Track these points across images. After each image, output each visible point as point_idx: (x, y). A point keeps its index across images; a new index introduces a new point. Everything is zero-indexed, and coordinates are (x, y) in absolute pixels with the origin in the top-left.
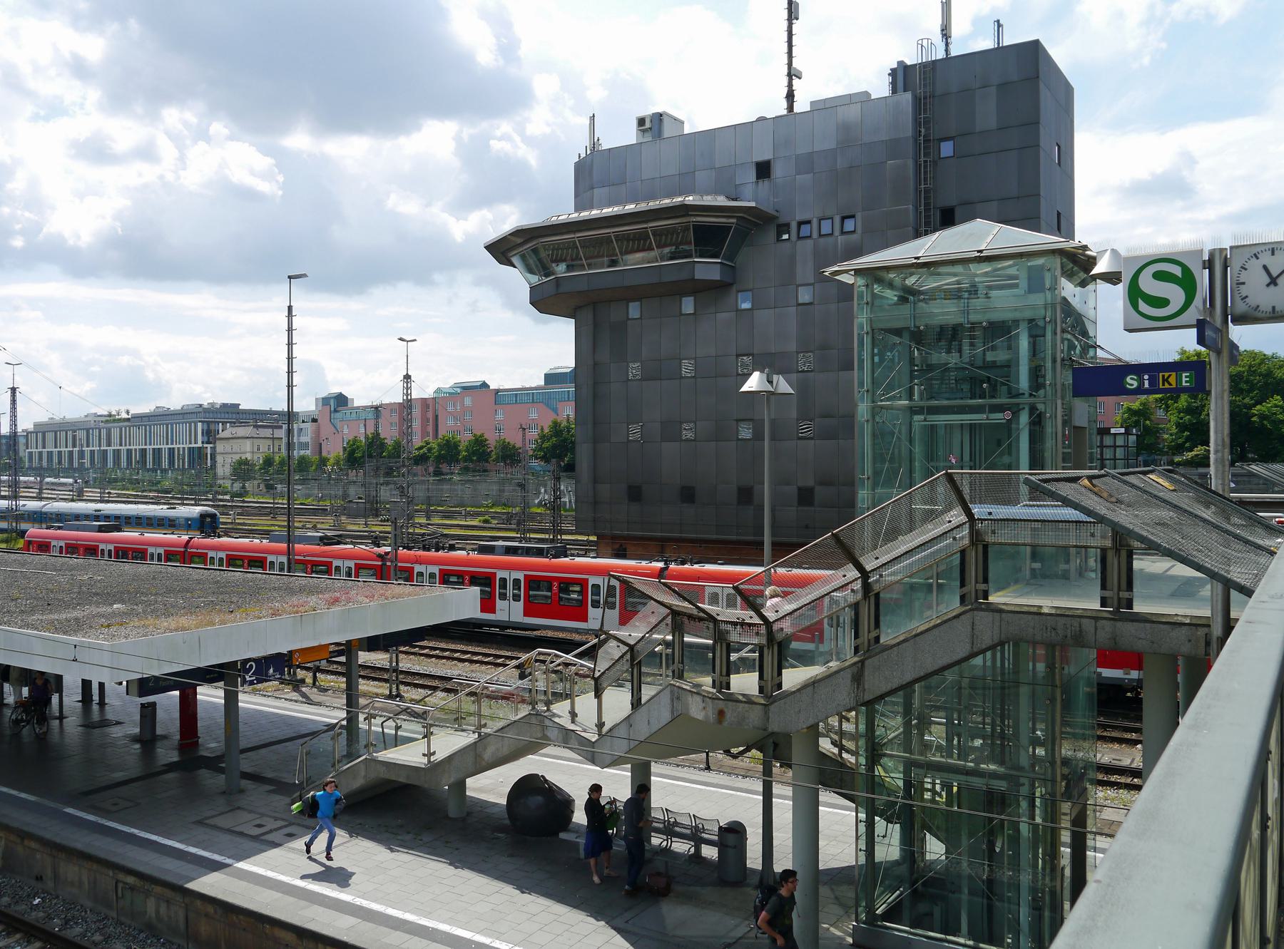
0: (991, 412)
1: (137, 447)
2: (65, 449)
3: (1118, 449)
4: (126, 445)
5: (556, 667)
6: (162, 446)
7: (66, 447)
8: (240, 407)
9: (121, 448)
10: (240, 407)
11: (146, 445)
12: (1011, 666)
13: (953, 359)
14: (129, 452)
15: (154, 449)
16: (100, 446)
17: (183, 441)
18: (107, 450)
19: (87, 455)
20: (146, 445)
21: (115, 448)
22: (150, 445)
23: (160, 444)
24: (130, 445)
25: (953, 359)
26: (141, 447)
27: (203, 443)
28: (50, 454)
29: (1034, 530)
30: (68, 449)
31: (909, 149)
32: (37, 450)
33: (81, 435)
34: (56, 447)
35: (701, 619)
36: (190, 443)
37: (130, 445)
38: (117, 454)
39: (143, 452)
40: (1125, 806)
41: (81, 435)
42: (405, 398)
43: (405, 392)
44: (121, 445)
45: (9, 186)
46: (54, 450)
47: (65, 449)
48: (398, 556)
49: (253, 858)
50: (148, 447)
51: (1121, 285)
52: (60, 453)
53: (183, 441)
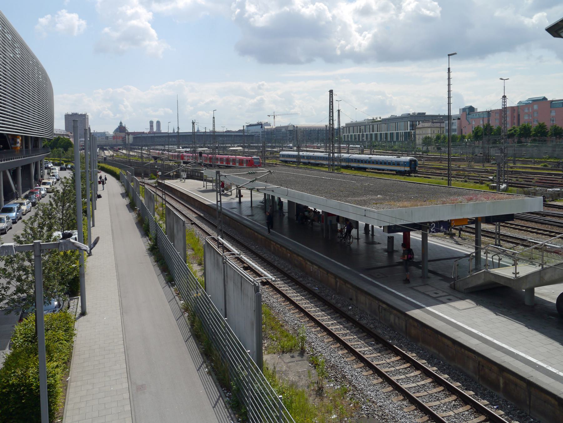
1: (384, 132)
8: (426, 114)
10: (426, 114)
11: (378, 131)
15: (390, 133)
16: (370, 132)
22: (389, 131)
27: (410, 130)
33: (363, 128)
36: (405, 130)
38: (363, 135)
41: (363, 128)
50: (388, 132)
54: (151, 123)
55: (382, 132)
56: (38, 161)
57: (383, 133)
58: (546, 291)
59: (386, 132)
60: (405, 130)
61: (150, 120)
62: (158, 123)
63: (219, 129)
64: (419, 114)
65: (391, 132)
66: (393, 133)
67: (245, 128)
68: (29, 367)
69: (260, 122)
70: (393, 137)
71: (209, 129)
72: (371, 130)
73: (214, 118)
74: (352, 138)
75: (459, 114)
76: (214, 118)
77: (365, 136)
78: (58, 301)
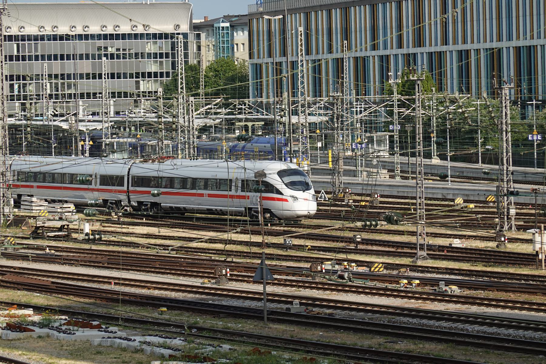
0: (227, 195)
1: (482, 46)
2: (395, 51)
4: (455, 42)
5: (167, 118)
6: (535, 42)
7: (400, 46)
9: (444, 48)
13: (233, 136)
18: (415, 55)
20: (500, 39)
21: (433, 49)
23: (532, 38)
24: (465, 42)
25: (233, 136)
26: (488, 45)
30: (405, 51)
32: (330, 57)
34: (374, 47)
35: (240, 168)
40: (94, 114)
44: (445, 42)
45: (205, 34)
46: (370, 53)
47: (395, 51)
50: (504, 44)
51: (86, 232)
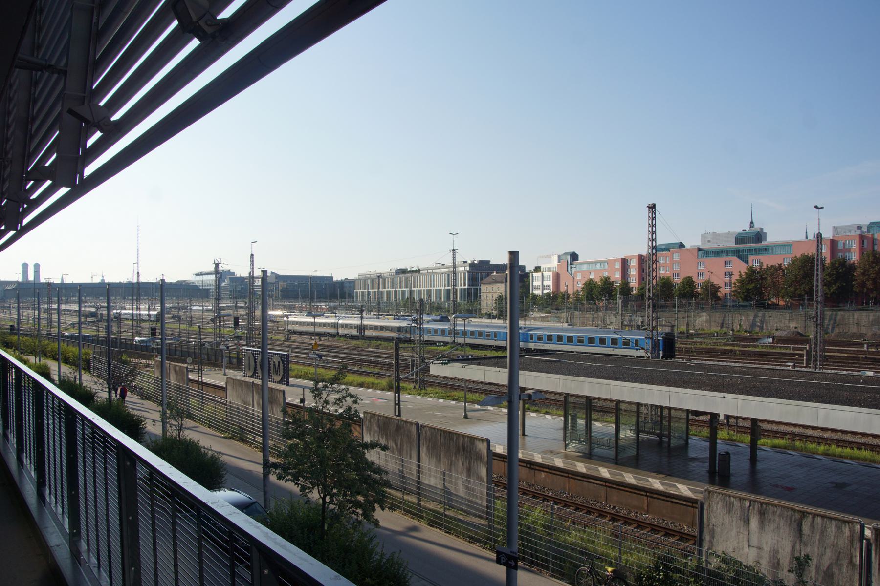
1: (425, 288)
3: (463, 339)
8: (491, 263)
10: (491, 263)
11: (431, 287)
12: (14, 381)
14: (420, 292)
15: (436, 290)
16: (379, 288)
17: (434, 284)
19: (372, 294)
22: (434, 287)
27: (469, 285)
28: (389, 293)
29: (271, 402)
31: (38, 282)
33: (369, 282)
34: (393, 288)
36: (445, 286)
37: (420, 287)
38: (369, 293)
39: (429, 292)
41: (369, 282)
42: (650, 243)
43: (650, 237)
48: (621, 443)
49: (19, 487)
50: (432, 288)
52: (396, 291)
53: (434, 284)
54: (25, 266)
55: (421, 288)
56: (663, 357)
57: (424, 290)
58: (478, 415)
59: (429, 288)
60: (445, 286)
61: (24, 262)
62: (37, 267)
63: (143, 279)
64: (481, 262)
65: (437, 288)
66: (390, 291)
67: (633, 272)
68: (611, 572)
69: (802, 256)
70: (413, 294)
71: (59, 281)
72: (403, 284)
73: (252, 255)
74: (390, 298)
75: (520, 264)
76: (252, 255)
77: (372, 294)
78: (332, 489)
